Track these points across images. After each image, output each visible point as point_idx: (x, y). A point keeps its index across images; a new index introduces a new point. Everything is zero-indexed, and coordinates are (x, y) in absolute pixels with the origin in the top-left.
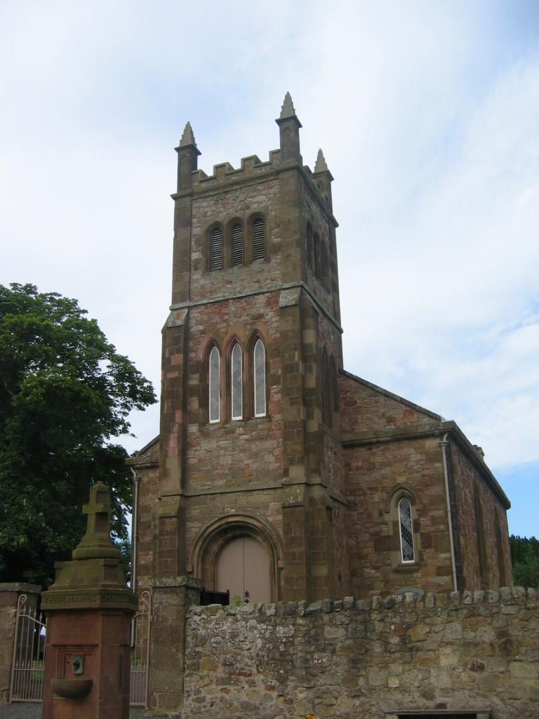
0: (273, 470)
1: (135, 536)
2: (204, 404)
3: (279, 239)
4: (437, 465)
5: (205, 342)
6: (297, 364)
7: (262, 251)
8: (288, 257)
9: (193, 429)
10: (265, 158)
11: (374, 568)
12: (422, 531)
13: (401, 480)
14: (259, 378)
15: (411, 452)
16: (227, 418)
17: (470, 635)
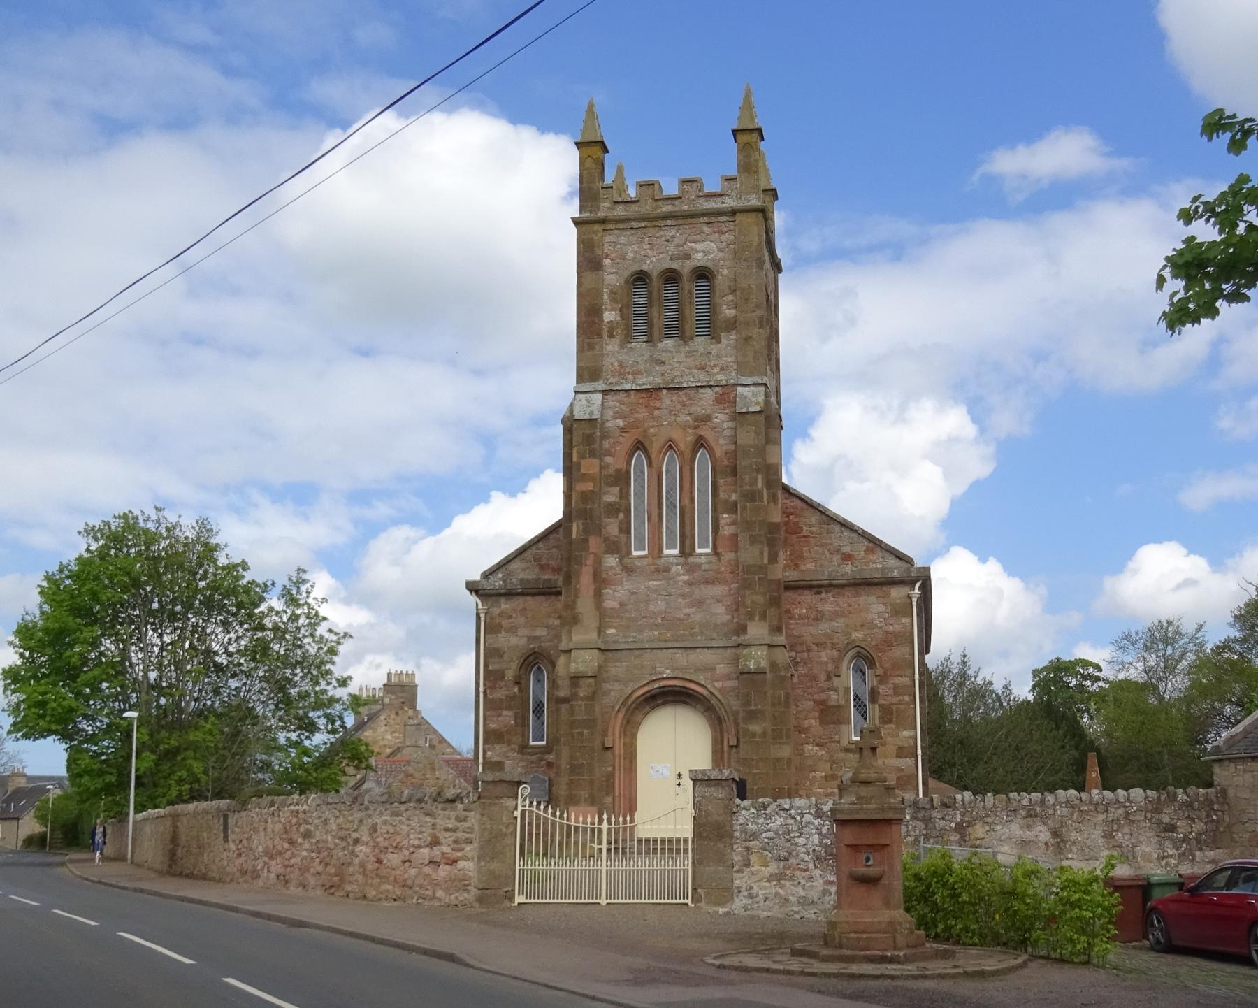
0: (723, 624)
1: (481, 689)
3: (733, 312)
4: (905, 620)
5: (627, 441)
6: (760, 493)
8: (747, 339)
11: (817, 745)
12: (881, 702)
13: (857, 635)
16: (656, 550)
17: (1028, 835)
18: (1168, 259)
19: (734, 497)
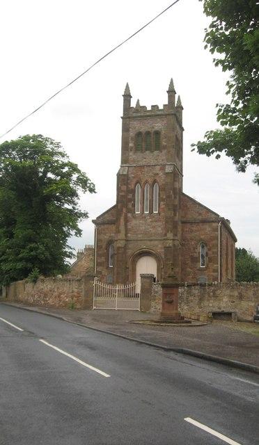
2: (134, 205)
4: (216, 233)
5: (135, 181)
7: (158, 147)
9: (129, 215)
10: (161, 107)
14: (156, 198)
15: (207, 228)
17: (231, 294)
18: (199, 142)
19: (164, 197)
